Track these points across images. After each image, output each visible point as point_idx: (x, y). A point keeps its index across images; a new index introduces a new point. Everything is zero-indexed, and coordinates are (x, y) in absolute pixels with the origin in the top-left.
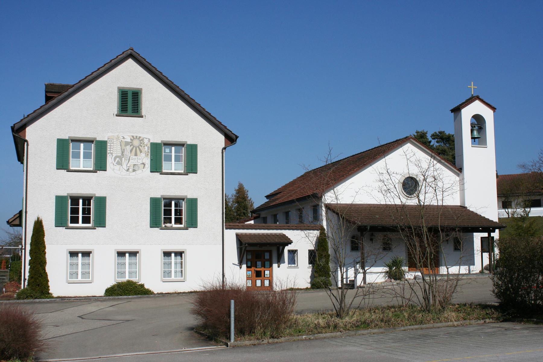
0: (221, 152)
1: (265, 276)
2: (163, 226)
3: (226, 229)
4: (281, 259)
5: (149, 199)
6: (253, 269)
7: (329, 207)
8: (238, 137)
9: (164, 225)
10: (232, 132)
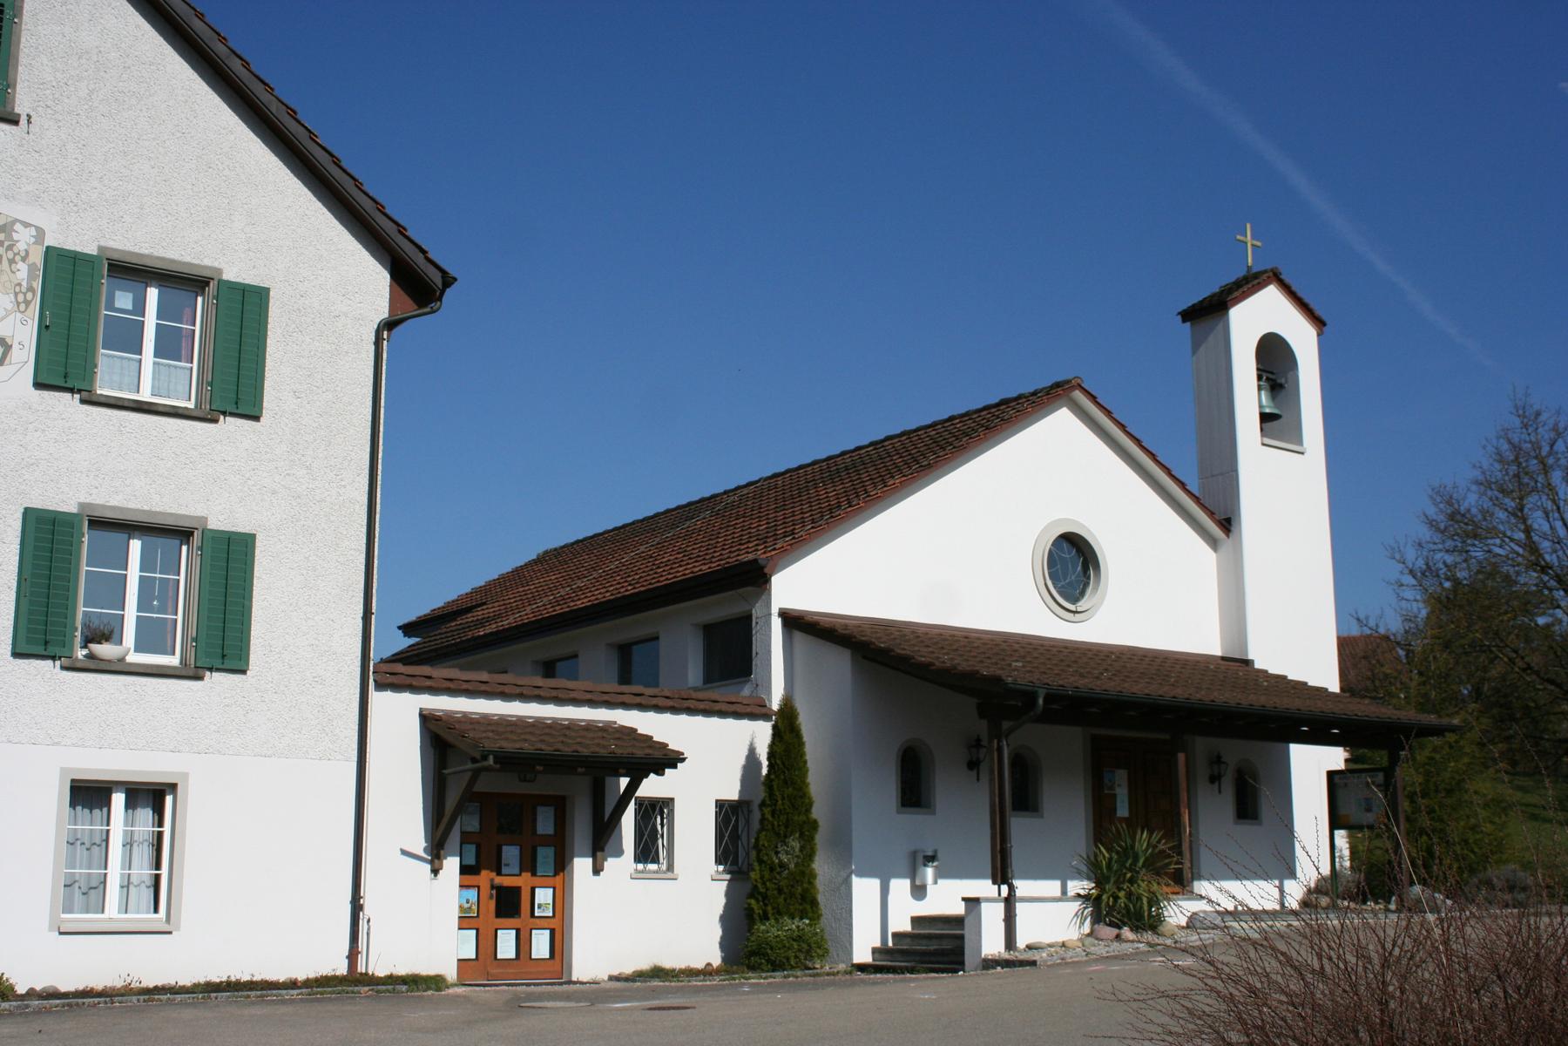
0: (373, 338)
1: (536, 914)
2: (81, 653)
3: (380, 686)
4: (610, 841)
5: (19, 515)
6: (486, 876)
7: (795, 622)
8: (455, 279)
9: (85, 652)
10: (430, 255)
